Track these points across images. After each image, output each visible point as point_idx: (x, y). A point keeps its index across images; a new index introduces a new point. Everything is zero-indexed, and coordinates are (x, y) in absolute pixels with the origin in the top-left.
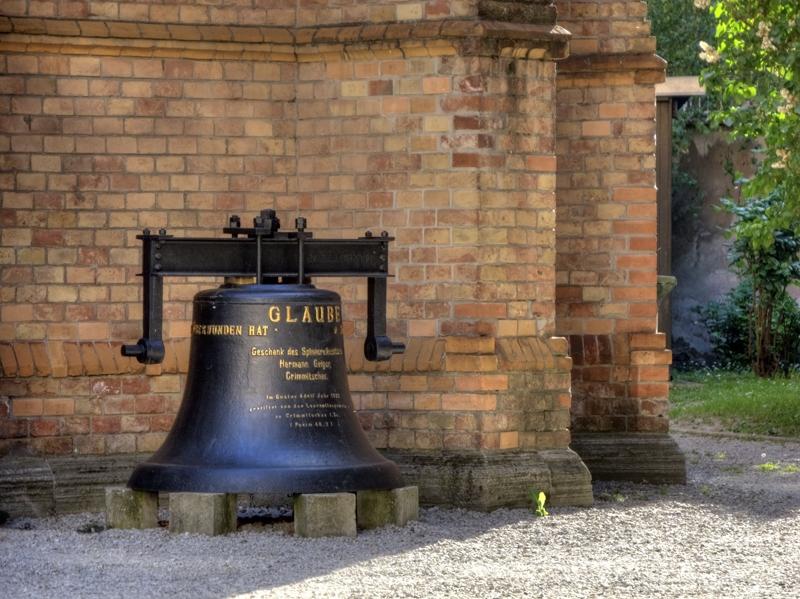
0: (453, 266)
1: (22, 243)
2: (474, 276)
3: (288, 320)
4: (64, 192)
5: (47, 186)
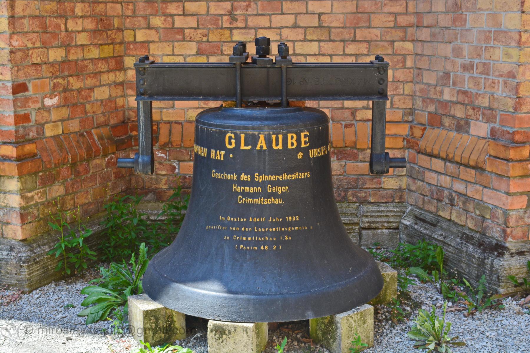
0: (501, 80)
1: (189, 52)
2: (514, 91)
3: (243, 147)
4: (221, 15)
5: (208, 11)
